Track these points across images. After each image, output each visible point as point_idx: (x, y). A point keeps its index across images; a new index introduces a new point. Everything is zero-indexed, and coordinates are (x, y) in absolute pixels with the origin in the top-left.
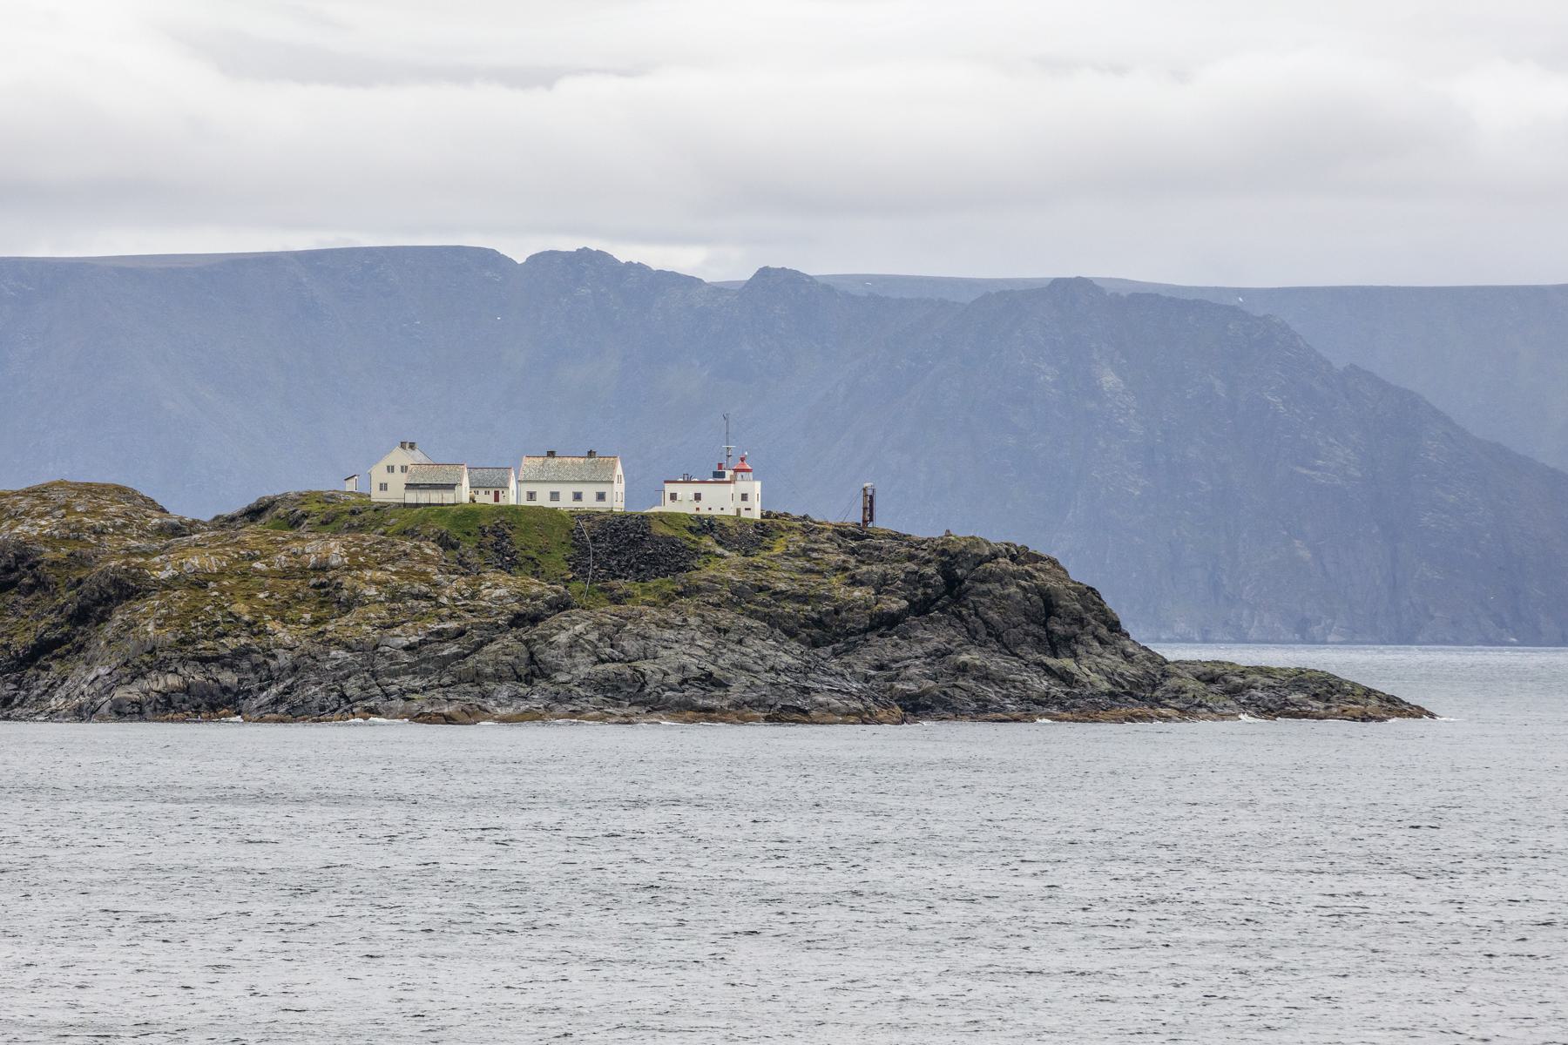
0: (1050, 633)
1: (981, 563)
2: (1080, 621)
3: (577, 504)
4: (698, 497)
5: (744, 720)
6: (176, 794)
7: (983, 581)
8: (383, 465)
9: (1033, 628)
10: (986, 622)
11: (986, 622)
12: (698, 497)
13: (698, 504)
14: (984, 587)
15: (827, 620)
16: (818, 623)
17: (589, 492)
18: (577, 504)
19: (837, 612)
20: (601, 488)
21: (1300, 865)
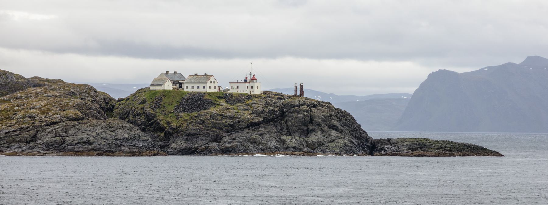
0: (308, 129)
1: (294, 107)
2: (319, 125)
3: (198, 90)
4: (238, 87)
5: (91, 155)
6: (381, 185)
7: (292, 113)
8: (209, 82)
9: (303, 127)
10: (287, 126)
11: (287, 126)
12: (238, 87)
13: (237, 90)
14: (292, 115)
15: (235, 125)
16: (232, 126)
17: (201, 86)
18: (198, 90)
19: (239, 122)
20: (204, 85)
21: (233, 193)
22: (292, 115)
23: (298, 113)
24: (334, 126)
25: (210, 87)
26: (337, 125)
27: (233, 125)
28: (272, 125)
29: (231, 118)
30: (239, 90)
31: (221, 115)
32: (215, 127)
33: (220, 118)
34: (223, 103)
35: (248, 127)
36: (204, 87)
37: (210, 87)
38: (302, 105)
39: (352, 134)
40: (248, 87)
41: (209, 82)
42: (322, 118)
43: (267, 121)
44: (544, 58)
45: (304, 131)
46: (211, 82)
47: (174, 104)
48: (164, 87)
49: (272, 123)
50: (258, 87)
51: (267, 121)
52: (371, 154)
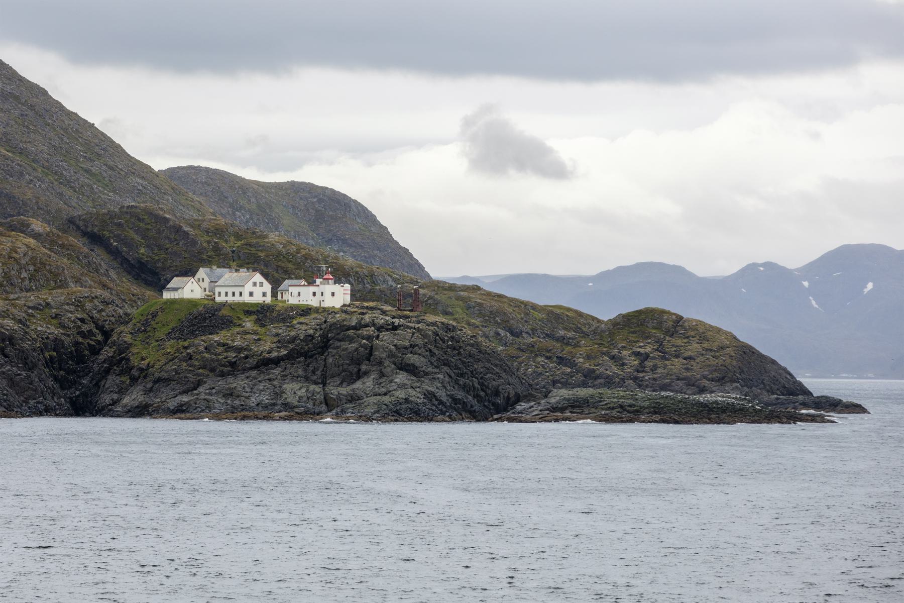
1: (348, 329)
2: (380, 363)
8: (250, 283)
16: (233, 364)
20: (240, 289)
22: (339, 344)
23: (351, 340)
24: (409, 365)
25: (251, 294)
26: (417, 364)
27: (235, 362)
28: (299, 363)
29: (239, 350)
30: (301, 298)
31: (224, 345)
32: (204, 367)
33: (220, 350)
34: (249, 324)
35: (256, 367)
36: (241, 294)
37: (251, 294)
38: (367, 326)
39: (457, 382)
40: (314, 294)
41: (250, 283)
42: (391, 351)
43: (291, 357)
44: (73, 117)
45: (351, 374)
46: (255, 284)
47: (172, 325)
48: (182, 293)
49: (302, 359)
50: (333, 294)
51: (291, 357)
52: (82, 406)
